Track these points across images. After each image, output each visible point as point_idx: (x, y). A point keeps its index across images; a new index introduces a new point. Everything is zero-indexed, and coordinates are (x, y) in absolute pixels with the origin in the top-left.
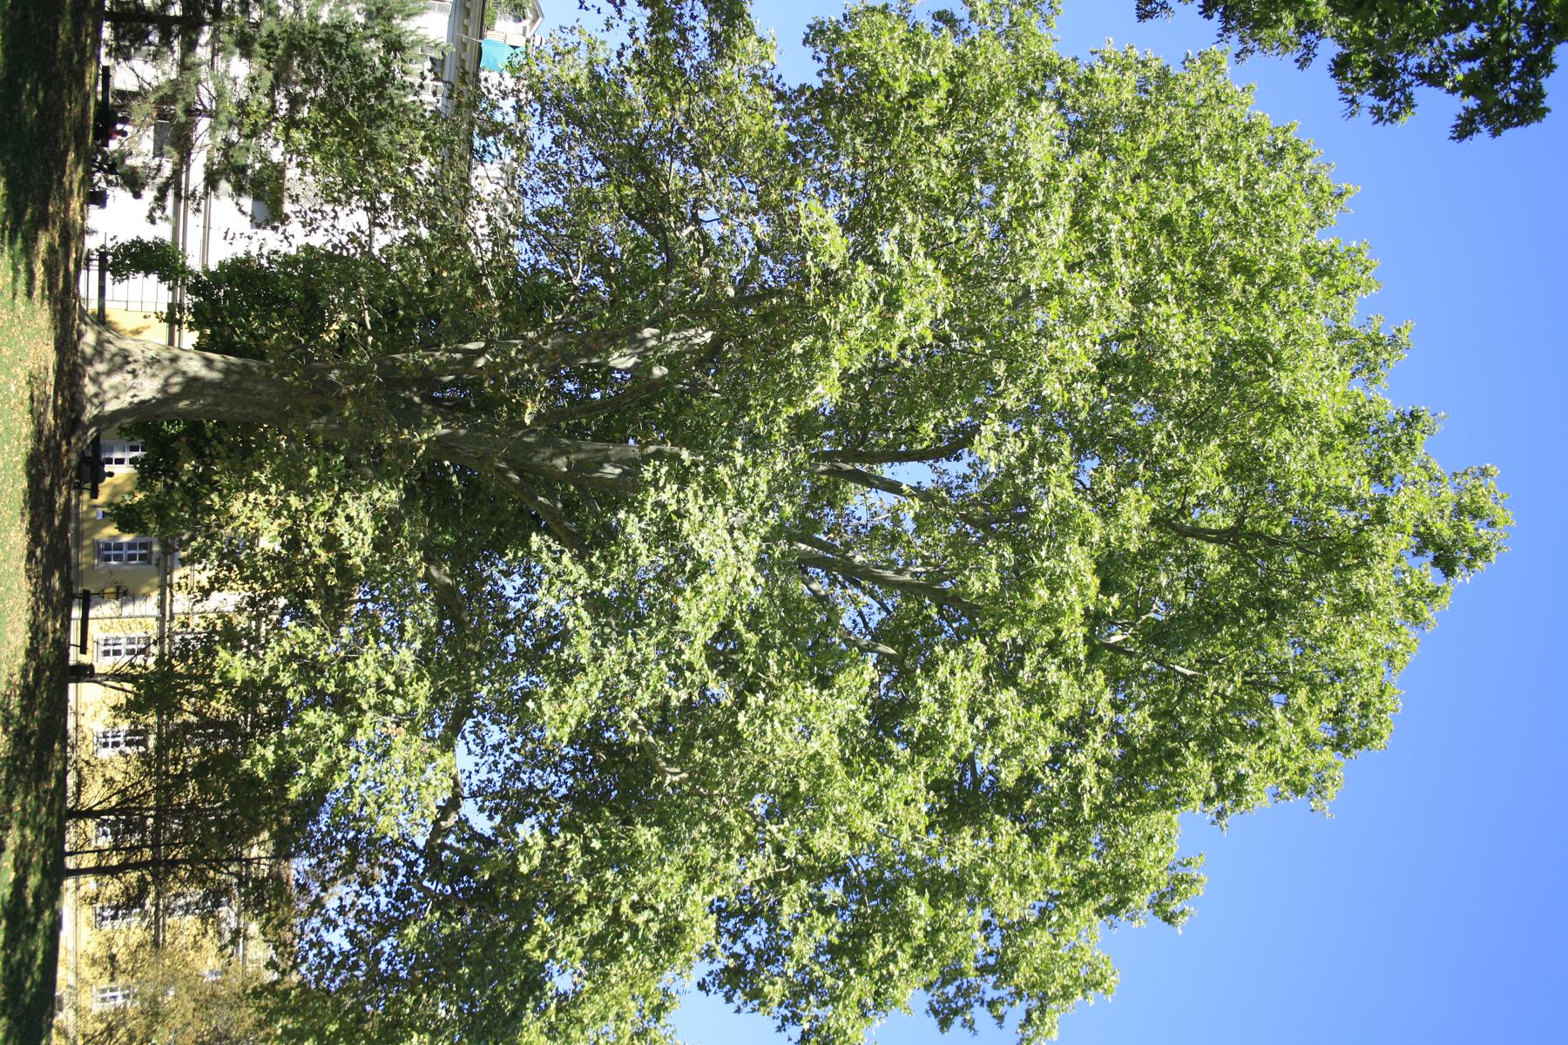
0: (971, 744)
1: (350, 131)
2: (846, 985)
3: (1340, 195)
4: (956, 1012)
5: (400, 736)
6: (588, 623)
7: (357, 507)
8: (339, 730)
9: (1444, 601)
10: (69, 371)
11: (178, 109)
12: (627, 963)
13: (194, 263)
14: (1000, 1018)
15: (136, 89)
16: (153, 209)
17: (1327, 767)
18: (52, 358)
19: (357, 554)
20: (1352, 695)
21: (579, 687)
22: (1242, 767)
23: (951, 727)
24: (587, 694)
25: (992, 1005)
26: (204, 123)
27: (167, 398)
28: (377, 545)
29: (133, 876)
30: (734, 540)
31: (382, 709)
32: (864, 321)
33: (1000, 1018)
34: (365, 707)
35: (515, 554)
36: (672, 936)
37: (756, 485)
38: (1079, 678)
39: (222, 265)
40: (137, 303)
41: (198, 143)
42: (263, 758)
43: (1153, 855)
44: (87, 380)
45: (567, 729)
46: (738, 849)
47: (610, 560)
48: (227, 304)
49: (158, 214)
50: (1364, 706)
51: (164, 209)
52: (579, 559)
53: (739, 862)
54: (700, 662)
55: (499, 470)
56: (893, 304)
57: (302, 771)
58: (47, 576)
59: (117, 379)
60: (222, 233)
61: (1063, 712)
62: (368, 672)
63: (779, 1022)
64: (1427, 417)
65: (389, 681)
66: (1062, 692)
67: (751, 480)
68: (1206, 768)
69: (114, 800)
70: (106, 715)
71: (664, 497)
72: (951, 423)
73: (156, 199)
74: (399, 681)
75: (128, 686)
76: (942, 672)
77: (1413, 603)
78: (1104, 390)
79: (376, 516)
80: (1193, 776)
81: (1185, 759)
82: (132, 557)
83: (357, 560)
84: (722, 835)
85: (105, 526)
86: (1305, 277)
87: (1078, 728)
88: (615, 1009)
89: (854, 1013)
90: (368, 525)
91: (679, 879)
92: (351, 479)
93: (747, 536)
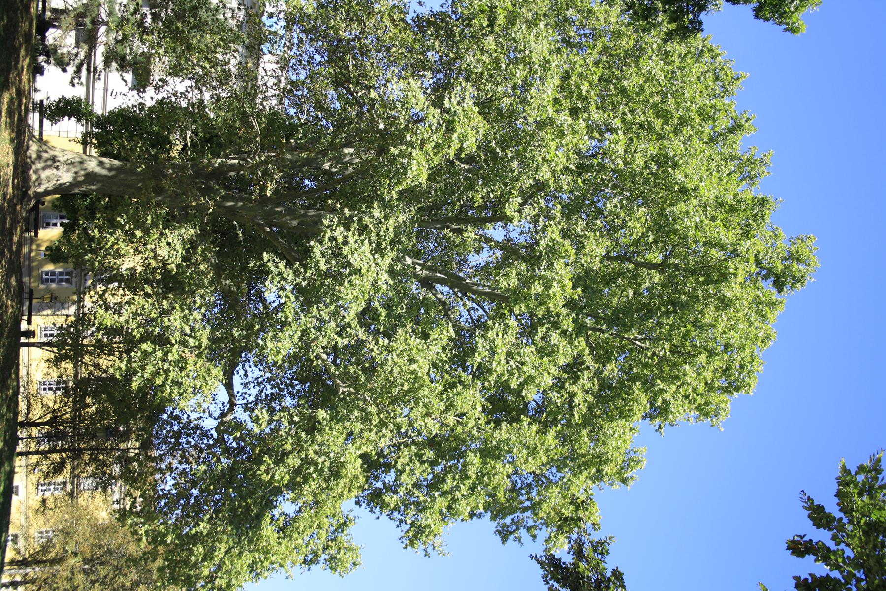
0: (506, 375)
1: (177, 35)
2: (432, 501)
3: (738, 79)
4: (511, 533)
5: (191, 358)
6: (293, 300)
7: (173, 237)
8: (159, 354)
9: (781, 308)
10: (22, 167)
11: (87, 20)
12: (312, 483)
13: (98, 109)
14: (534, 537)
15: (64, 8)
16: (73, 78)
17: (722, 402)
18: (11, 159)
19: (173, 262)
20: (734, 360)
21: (287, 334)
22: (668, 396)
23: (495, 364)
24: (291, 337)
25: (529, 529)
26: (103, 29)
27: (75, 184)
28: (184, 259)
29: (56, 456)
30: (375, 259)
31: (184, 343)
32: (435, 138)
33: (534, 537)
34: (174, 342)
35: (255, 264)
36: (336, 471)
37: (388, 229)
38: (571, 343)
39: (110, 112)
40: (64, 136)
41: (99, 40)
42: (120, 368)
43: (614, 444)
44: (31, 172)
45: (280, 356)
46: (375, 426)
47: (305, 267)
48: (111, 132)
49: (76, 81)
50: (742, 367)
51: (80, 78)
52: (289, 265)
53: (376, 434)
54: (354, 323)
55: (259, 224)
56: (450, 129)
57: (139, 374)
58: (9, 276)
59: (48, 173)
60: (115, 93)
61: (562, 361)
62: (175, 324)
63: (398, 523)
64: (771, 200)
65: (187, 329)
66: (561, 349)
67: (385, 226)
68: (644, 399)
69: (48, 417)
70: (44, 365)
71: (335, 234)
72: (491, 195)
73: (75, 72)
74: (192, 329)
75: (55, 349)
76: (491, 335)
77: (761, 308)
78: (580, 181)
79: (184, 243)
80: (637, 401)
81: (634, 392)
82: (61, 280)
83: (173, 266)
84: (366, 418)
85: (46, 264)
86: (698, 120)
87: (573, 369)
88: (317, 522)
89: (437, 517)
90: (179, 247)
91: (341, 439)
92: (170, 222)
93: (383, 258)
